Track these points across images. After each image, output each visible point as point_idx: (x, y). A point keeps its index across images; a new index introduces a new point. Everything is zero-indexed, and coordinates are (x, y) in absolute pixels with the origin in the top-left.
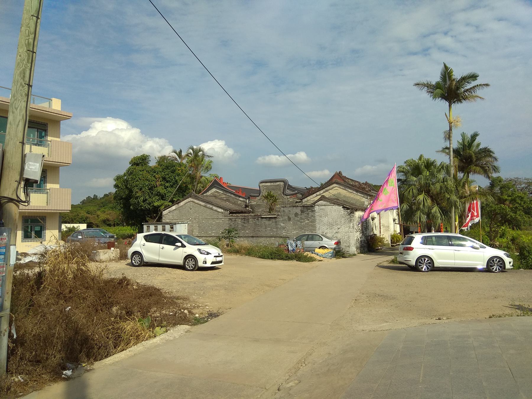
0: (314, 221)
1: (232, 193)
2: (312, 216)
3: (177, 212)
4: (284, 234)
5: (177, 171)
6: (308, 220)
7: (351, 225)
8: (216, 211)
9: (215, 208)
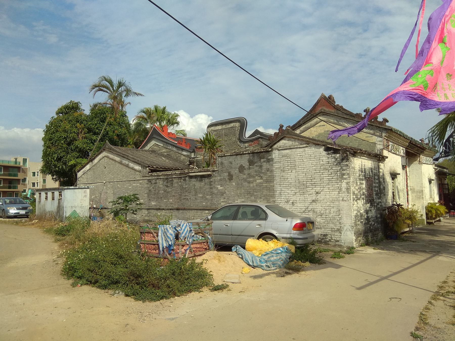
0: (271, 180)
1: (174, 146)
2: (268, 170)
6: (261, 178)
7: (344, 185)
9: (131, 165)
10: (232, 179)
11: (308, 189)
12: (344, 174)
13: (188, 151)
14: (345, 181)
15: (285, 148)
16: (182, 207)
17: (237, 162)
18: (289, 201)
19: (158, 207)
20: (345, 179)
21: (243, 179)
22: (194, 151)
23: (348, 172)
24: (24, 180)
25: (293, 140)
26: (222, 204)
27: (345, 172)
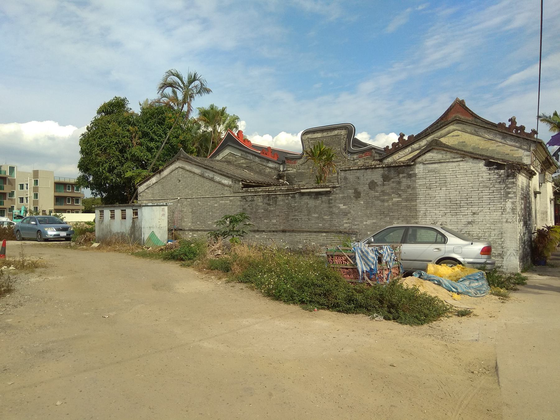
0: (413, 198)
1: (255, 156)
2: (409, 187)
3: (158, 186)
4: (346, 225)
5: (167, 121)
6: (400, 196)
7: (509, 205)
8: (219, 183)
9: (218, 178)
10: (360, 197)
11: (462, 209)
12: (509, 193)
13: (275, 162)
14: (510, 200)
15: (433, 162)
16: (290, 228)
17: (367, 177)
18: (437, 222)
19: (256, 229)
20: (511, 198)
21: (375, 197)
22: (283, 163)
23: (514, 190)
24: (12, 194)
25: (443, 152)
26: (345, 225)
27: (510, 190)
